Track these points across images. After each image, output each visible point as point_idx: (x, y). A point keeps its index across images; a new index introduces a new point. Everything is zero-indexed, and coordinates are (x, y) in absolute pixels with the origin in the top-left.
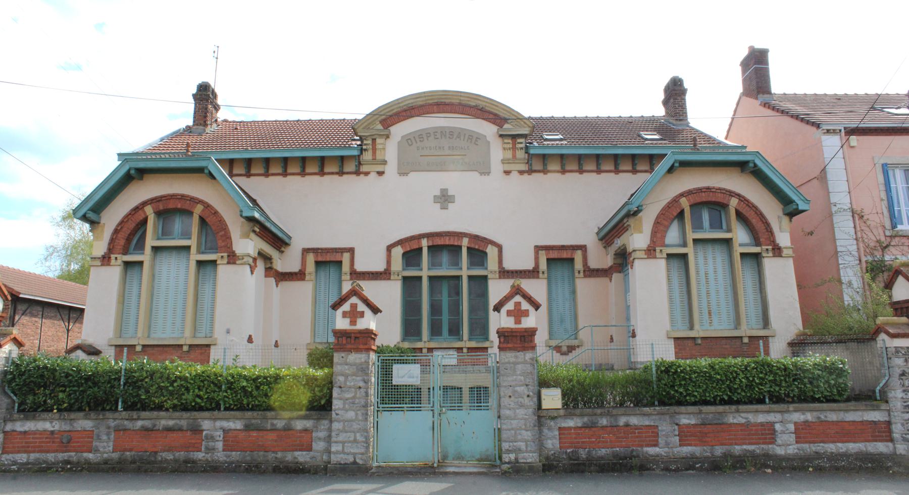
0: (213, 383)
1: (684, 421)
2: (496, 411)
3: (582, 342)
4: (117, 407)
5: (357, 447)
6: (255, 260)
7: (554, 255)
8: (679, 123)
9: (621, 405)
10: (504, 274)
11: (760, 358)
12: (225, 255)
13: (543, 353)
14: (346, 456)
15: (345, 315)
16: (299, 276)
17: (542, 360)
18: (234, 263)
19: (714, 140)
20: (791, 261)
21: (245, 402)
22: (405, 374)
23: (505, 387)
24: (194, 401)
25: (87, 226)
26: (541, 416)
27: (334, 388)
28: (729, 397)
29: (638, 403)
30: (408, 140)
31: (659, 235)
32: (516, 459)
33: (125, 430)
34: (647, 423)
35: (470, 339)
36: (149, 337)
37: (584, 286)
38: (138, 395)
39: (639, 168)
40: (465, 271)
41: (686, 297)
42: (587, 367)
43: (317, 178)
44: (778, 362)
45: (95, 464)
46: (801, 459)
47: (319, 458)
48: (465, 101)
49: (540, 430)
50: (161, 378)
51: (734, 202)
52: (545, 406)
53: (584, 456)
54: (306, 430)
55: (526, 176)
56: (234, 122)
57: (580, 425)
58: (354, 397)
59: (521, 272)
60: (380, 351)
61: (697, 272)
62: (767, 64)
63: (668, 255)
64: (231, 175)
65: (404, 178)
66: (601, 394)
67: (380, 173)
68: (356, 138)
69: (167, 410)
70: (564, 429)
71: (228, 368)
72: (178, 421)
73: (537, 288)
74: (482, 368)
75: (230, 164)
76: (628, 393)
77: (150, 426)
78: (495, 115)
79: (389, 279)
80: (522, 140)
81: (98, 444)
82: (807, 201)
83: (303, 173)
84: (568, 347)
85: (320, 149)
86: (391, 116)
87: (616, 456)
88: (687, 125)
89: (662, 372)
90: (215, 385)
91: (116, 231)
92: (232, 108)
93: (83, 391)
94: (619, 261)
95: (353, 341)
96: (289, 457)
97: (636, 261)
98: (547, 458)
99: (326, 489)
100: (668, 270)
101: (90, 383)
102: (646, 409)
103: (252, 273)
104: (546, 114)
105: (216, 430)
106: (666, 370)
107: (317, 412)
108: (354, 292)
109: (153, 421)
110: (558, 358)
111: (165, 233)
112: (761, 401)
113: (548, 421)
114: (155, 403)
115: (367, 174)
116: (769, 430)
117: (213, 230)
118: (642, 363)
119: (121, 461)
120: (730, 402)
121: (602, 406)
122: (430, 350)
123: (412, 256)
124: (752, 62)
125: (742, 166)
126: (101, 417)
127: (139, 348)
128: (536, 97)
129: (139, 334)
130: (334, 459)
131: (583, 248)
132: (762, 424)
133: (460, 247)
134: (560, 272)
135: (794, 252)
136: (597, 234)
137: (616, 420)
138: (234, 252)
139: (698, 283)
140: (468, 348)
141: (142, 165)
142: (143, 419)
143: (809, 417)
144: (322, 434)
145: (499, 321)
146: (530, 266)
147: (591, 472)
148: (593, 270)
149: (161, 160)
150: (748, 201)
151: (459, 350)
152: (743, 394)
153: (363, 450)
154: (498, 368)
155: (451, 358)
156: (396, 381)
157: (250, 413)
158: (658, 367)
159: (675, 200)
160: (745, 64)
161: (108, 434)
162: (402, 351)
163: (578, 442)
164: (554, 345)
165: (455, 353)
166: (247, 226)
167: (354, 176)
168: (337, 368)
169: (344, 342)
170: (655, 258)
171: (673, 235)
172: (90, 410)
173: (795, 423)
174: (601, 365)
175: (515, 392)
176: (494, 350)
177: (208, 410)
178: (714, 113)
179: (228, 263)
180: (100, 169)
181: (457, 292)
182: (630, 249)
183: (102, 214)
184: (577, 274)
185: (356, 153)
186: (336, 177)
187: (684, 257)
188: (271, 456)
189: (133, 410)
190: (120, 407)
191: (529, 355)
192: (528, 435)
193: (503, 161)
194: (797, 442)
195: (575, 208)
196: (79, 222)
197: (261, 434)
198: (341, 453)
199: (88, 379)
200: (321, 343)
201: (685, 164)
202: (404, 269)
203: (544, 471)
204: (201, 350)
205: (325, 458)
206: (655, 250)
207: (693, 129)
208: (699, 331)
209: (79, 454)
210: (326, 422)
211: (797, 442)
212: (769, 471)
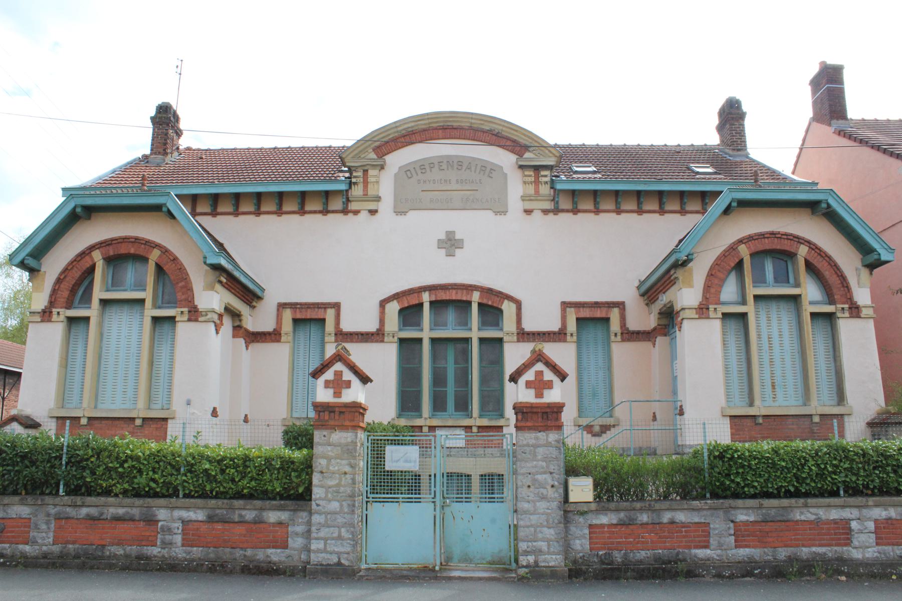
0: (170, 464)
1: (742, 517)
3: (618, 420)
4: (58, 490)
5: (343, 546)
6: (220, 316)
7: (586, 313)
8: (736, 153)
9: (666, 497)
10: (524, 336)
11: (834, 441)
12: (186, 310)
13: (573, 436)
14: (328, 556)
15: (327, 384)
16: (274, 336)
17: (570, 442)
18: (196, 320)
19: (779, 174)
20: (871, 323)
21: (208, 488)
22: (401, 458)
23: (523, 474)
24: (148, 485)
25: (26, 275)
27: (315, 474)
28: (796, 488)
29: (686, 495)
30: (407, 171)
31: (713, 290)
32: (536, 562)
33: (67, 518)
34: (696, 520)
35: (481, 416)
36: (96, 407)
37: (621, 351)
38: (83, 477)
39: (581, 206)
40: (475, 333)
41: (745, 365)
42: (624, 452)
44: (855, 446)
45: (33, 558)
46: (882, 564)
47: (296, 558)
48: (476, 124)
49: (567, 529)
50: (109, 457)
51: (803, 251)
52: (572, 499)
54: (280, 523)
55: (551, 215)
56: (199, 150)
57: (615, 522)
58: (338, 485)
59: (544, 333)
60: (370, 429)
61: (759, 336)
62: (842, 83)
63: (723, 314)
64: (194, 214)
66: (641, 484)
67: (373, 212)
68: (344, 169)
69: (116, 495)
70: (596, 526)
71: (188, 447)
72: (129, 510)
73: (563, 354)
74: (495, 451)
75: (193, 200)
76: (673, 483)
77: (96, 514)
78: (514, 141)
79: (382, 341)
80: (547, 173)
81: (35, 534)
82: (891, 250)
83: (279, 212)
84: (601, 426)
85: (300, 182)
86: (387, 142)
87: (657, 559)
88: (747, 156)
89: (715, 457)
90: (173, 467)
91: (59, 281)
92: (194, 136)
93: (19, 472)
94: (664, 322)
95: (337, 417)
96: (260, 555)
97: (685, 322)
98: (575, 562)
99: (309, 592)
100: (724, 333)
101: (26, 462)
102: (696, 503)
103: (217, 333)
104: (576, 141)
105: (174, 521)
106: (720, 455)
107: (294, 502)
108: (339, 357)
109: (99, 509)
110: (589, 441)
111: (116, 283)
112: (834, 494)
113: (577, 517)
114: (101, 487)
115: (356, 212)
116: (843, 529)
117: (170, 277)
118: (691, 446)
119: (62, 556)
120: (797, 494)
121: (642, 499)
123: (410, 313)
124: (824, 81)
125: (812, 207)
126: (39, 502)
127: (84, 421)
128: (565, 120)
129: (85, 405)
130: (315, 558)
131: (621, 305)
132: (835, 522)
133: (469, 303)
134: (593, 333)
135: (875, 312)
136: (638, 288)
138: (195, 307)
139: (760, 349)
140: (479, 427)
141: (89, 202)
142: (89, 506)
143: (892, 513)
144: (300, 529)
145: (517, 394)
146: (555, 326)
147: (627, 579)
148: (633, 333)
149: (112, 195)
150: (820, 249)
151: (468, 428)
152: (813, 484)
154: (514, 452)
155: (458, 439)
156: (389, 466)
157: (213, 502)
158: (711, 452)
159: (733, 248)
160: (816, 83)
161: (48, 523)
162: (397, 430)
163: (612, 543)
164: (585, 424)
165: (463, 432)
166: (212, 275)
167: (340, 215)
168: (318, 450)
169: (327, 418)
170: (708, 318)
171: (729, 290)
172: (27, 494)
173: (876, 521)
174: (640, 448)
175: (535, 480)
176: (510, 430)
177: (164, 496)
178: (778, 142)
179: (189, 320)
180: (40, 207)
181: (465, 355)
182: (677, 307)
183: (43, 260)
184: (613, 337)
186: (319, 216)
187: (743, 316)
188: (238, 553)
189: (76, 495)
190: (61, 490)
191: (552, 436)
192: (550, 533)
193: (524, 198)
194: (877, 544)
195: (613, 256)
196: (18, 269)
197: (227, 526)
198: (325, 548)
199: (24, 457)
201: (744, 204)
202: (400, 330)
203: (570, 577)
204: (157, 424)
206: (708, 309)
207: (754, 161)
208: (760, 409)
209: (14, 546)
210: (304, 514)
211: (877, 544)
212: (843, 578)
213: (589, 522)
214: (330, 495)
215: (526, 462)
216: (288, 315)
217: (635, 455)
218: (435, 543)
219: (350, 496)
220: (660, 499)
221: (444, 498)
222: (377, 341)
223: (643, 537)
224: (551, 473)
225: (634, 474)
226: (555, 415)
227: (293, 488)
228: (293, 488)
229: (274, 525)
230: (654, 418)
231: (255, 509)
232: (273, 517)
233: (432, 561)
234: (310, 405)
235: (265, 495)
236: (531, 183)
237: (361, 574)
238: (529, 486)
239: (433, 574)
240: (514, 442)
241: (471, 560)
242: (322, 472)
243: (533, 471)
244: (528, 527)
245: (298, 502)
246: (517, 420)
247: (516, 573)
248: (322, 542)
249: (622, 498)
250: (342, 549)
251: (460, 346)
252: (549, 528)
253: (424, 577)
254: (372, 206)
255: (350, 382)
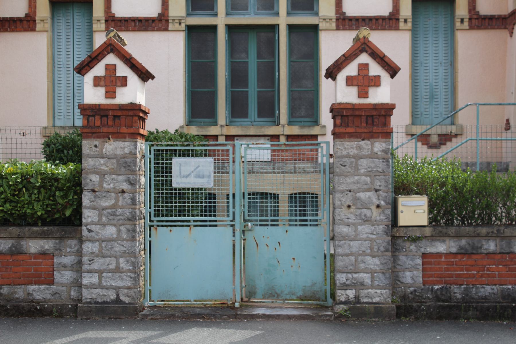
3: (462, 127)
5: (122, 279)
10: (345, 22)
13: (403, 145)
14: (104, 292)
15: (97, 82)
17: (400, 154)
22: (190, 172)
23: (342, 192)
27: (85, 193)
32: (357, 297)
35: (290, 123)
49: (395, 259)
52: (403, 221)
54: (43, 254)
57: (454, 250)
58: (114, 206)
60: (152, 138)
66: (488, 206)
70: (431, 255)
73: (395, 44)
74: (308, 166)
79: (166, 29)
95: (110, 123)
96: (20, 292)
98: (404, 297)
107: (60, 228)
108: (110, 48)
113: (407, 244)
121: (488, 223)
130: (87, 295)
137: (509, 245)
144: (68, 260)
145: (336, 92)
147: (468, 319)
151: (275, 137)
153: (129, 283)
155: (261, 152)
156: (177, 182)
163: (451, 276)
168: (88, 163)
169: (98, 123)
174: (489, 164)
175: (356, 199)
181: (270, 47)
184: (458, 24)
191: (379, 146)
192: (374, 263)
198: (99, 284)
200: (64, 128)
202: (188, 15)
203: (398, 315)
205: (73, 293)
210: (73, 242)
213: (423, 250)
214: (104, 218)
215: (346, 176)
217: (481, 170)
218: (234, 276)
219: (129, 220)
220: (511, 224)
221: (245, 220)
222: (159, 30)
223: (488, 270)
224: (377, 191)
225: (480, 192)
226: (382, 119)
227: (58, 211)
228: (58, 211)
229: (36, 256)
230: (508, 127)
231: (11, 238)
232: (33, 246)
233: (231, 296)
234: (76, 107)
235: (23, 220)
237: (145, 312)
238: (349, 206)
239: (233, 312)
240: (331, 152)
241: (278, 295)
242: (94, 191)
243: (354, 187)
244: (347, 255)
245: (65, 228)
246: (335, 125)
247: (332, 310)
248: (96, 275)
249: (463, 223)
250: (120, 284)
251: (264, 35)
252: (374, 257)
253: (221, 315)
255: (125, 78)
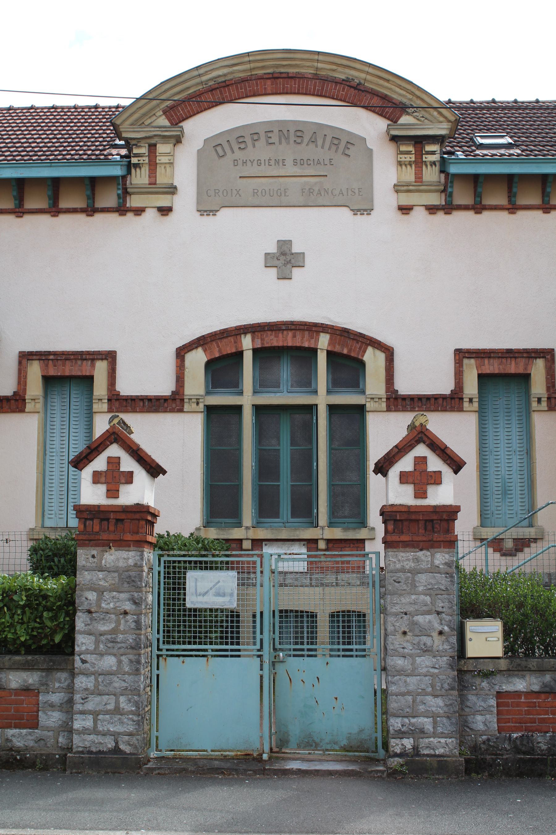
2: (377, 659)
7: (492, 367)
10: (396, 402)
14: (100, 739)
15: (97, 478)
22: (209, 589)
23: (396, 614)
26: (465, 670)
27: (79, 614)
30: (217, 146)
32: (415, 748)
35: (331, 524)
43: (45, 220)
48: (325, 69)
52: (472, 650)
53: (544, 747)
54: (26, 690)
55: (440, 216)
57: (536, 688)
58: (115, 631)
60: (164, 545)
65: (208, 220)
67: (165, 211)
68: (118, 142)
73: (457, 431)
74: (353, 577)
78: (384, 97)
79: (181, 411)
80: (435, 148)
85: (51, 164)
95: (112, 528)
98: (475, 748)
99: (64, 796)
104: (481, 95)
107: (47, 658)
110: (497, 564)
113: (478, 681)
115: (139, 211)
122: (257, 543)
123: (223, 369)
133: (314, 351)
134: (505, 399)
140: (328, 541)
144: (56, 698)
145: (387, 492)
151: (311, 543)
153: (131, 728)
154: (382, 580)
156: (193, 601)
162: (205, 546)
164: (490, 537)
165: (304, 550)
168: (84, 577)
169: (97, 528)
176: (375, 546)
184: (534, 405)
185: (117, 171)
186: (82, 217)
191: (441, 558)
192: (437, 704)
193: (398, 188)
198: (96, 726)
202: (208, 393)
203: (468, 771)
210: (63, 676)
216: (35, 371)
236: (410, 164)
254: (163, 201)
